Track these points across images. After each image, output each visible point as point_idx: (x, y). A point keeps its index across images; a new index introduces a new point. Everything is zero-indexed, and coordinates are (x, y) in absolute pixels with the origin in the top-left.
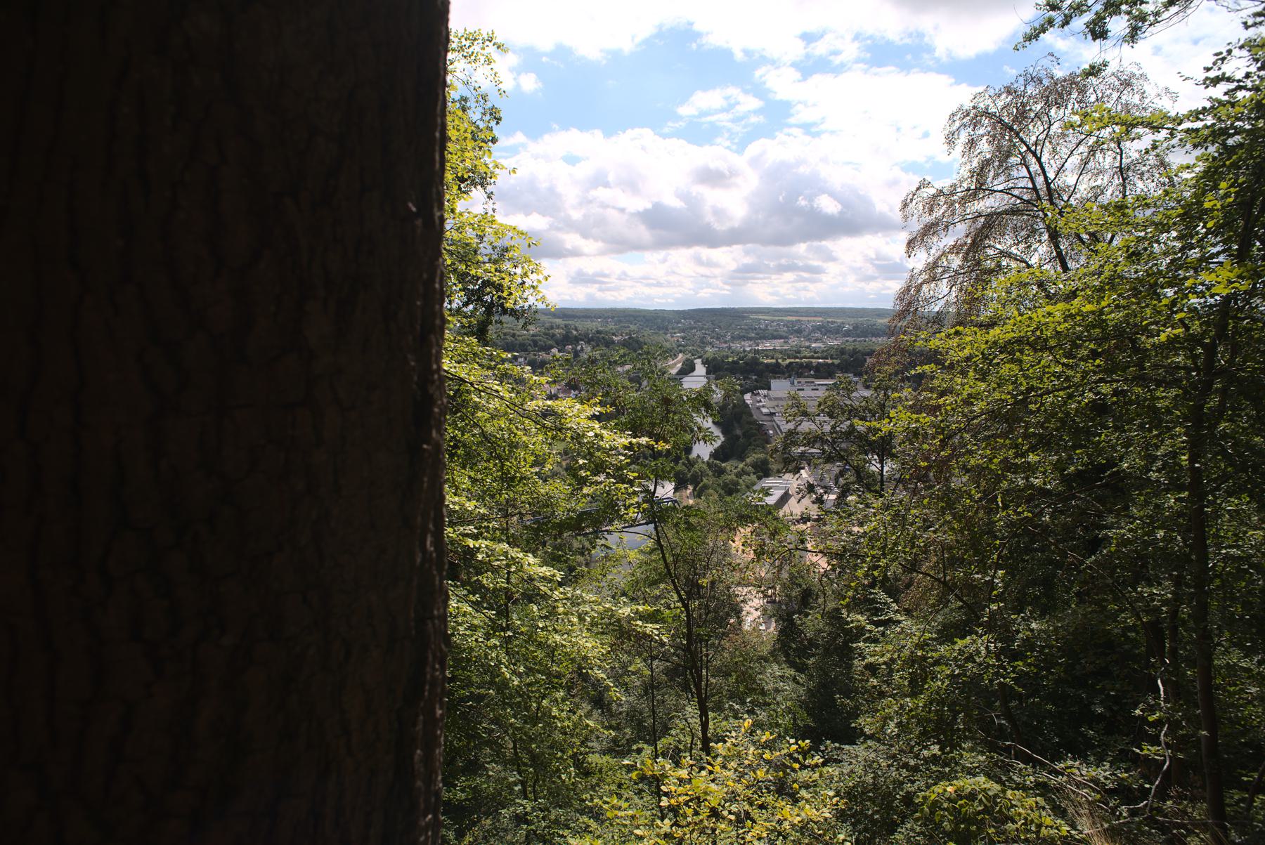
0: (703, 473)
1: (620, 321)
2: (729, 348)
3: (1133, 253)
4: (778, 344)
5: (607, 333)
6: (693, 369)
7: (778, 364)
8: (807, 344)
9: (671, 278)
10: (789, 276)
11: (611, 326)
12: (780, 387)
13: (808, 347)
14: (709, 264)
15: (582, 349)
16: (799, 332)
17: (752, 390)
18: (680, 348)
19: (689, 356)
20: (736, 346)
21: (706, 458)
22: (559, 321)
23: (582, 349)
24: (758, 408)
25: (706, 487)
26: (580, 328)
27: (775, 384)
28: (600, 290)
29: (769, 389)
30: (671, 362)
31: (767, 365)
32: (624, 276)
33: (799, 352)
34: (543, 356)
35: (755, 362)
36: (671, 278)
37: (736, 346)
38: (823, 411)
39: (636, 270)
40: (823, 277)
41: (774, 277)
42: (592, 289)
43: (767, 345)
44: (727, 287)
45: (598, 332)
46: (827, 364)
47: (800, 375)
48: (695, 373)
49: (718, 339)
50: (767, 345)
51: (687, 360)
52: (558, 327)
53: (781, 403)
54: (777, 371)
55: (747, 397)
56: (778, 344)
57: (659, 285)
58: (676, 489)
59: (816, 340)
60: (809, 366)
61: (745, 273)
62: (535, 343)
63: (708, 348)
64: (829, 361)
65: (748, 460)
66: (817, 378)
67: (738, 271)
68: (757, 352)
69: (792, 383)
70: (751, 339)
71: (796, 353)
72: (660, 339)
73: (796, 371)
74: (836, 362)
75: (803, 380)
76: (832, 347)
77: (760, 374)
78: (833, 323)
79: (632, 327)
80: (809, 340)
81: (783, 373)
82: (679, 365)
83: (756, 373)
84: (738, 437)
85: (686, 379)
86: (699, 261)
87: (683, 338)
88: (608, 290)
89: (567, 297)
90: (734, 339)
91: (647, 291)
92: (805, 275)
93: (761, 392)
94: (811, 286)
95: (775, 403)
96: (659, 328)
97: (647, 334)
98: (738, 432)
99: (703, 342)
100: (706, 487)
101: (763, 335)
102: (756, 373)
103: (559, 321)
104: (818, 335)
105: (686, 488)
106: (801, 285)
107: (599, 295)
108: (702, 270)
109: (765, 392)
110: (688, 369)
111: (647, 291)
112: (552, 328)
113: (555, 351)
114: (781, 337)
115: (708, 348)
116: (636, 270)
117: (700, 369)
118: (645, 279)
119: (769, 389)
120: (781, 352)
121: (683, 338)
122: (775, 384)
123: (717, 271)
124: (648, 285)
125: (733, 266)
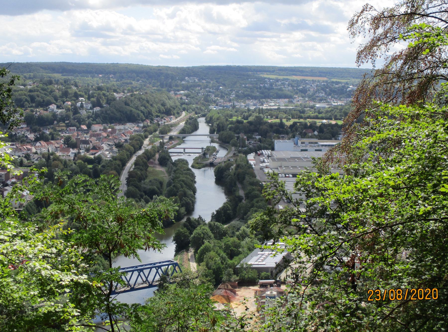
0: (205, 236)
1: (122, 77)
2: (234, 107)
3: (384, 210)
4: (282, 104)
5: (108, 89)
6: (195, 127)
7: (281, 125)
8: (312, 104)
9: (180, 34)
10: (298, 35)
11: (113, 82)
12: (284, 148)
13: (312, 107)
14: (221, 21)
15: (82, 106)
16: (304, 92)
17: (256, 150)
18: (184, 106)
19: (193, 115)
20: (241, 105)
21: (208, 219)
22: (57, 76)
23: (82, 106)
24: (262, 169)
25: (207, 250)
26: (80, 84)
27: (278, 144)
28: (105, 44)
29: (273, 149)
30: (174, 121)
31: (271, 126)
32: (130, 30)
33: (303, 112)
34: (40, 112)
35: (259, 122)
36: (180, 34)
37: (241, 105)
38: (299, 190)
39: (143, 25)
40: (333, 38)
41: (282, 35)
42: (96, 43)
43: (271, 105)
44: (236, 45)
45: (99, 89)
46: (330, 125)
47: (304, 135)
48: (198, 132)
49: (222, 97)
50: (271, 105)
51: (191, 118)
52: (57, 82)
53: (284, 164)
54: (280, 131)
55: (251, 157)
56: (282, 104)
57: (166, 40)
58: (178, 251)
59: (320, 101)
60: (313, 127)
61: (256, 30)
62: (33, 99)
63: (213, 107)
64: (333, 122)
65: (250, 222)
66: (321, 138)
67: (249, 28)
68: (261, 111)
69: (296, 144)
70: (255, 98)
71: (300, 113)
72: (164, 98)
73: (300, 131)
74: (340, 123)
75: (306, 140)
76: (336, 108)
77: (264, 134)
78: (337, 83)
79: (135, 84)
80: (314, 100)
81: (287, 133)
82: (182, 124)
83: (261, 133)
84: (240, 199)
85: (189, 138)
86: (209, 18)
87: (187, 96)
88: (112, 44)
89: (68, 51)
90: (238, 97)
91: (153, 46)
92: (313, 34)
93: (265, 152)
94: (319, 46)
95: (279, 164)
96: (162, 85)
97: (151, 90)
98: (241, 193)
99: (207, 101)
100: (207, 250)
101: (267, 93)
102: (261, 133)
103: (57, 76)
104: (322, 95)
105: (187, 251)
106: (310, 44)
107: (102, 49)
108: (209, 26)
109: (268, 152)
110: (192, 127)
111: (153, 46)
112: (50, 83)
113: (53, 107)
114: (285, 97)
115: (213, 107)
116: (143, 25)
117: (204, 128)
118: (149, 35)
119: (273, 149)
120: (285, 111)
121: (187, 96)
122: (278, 144)
123: (226, 28)
124: (155, 41)
125: (244, 23)
